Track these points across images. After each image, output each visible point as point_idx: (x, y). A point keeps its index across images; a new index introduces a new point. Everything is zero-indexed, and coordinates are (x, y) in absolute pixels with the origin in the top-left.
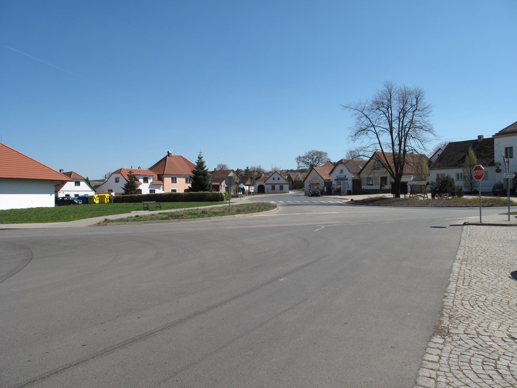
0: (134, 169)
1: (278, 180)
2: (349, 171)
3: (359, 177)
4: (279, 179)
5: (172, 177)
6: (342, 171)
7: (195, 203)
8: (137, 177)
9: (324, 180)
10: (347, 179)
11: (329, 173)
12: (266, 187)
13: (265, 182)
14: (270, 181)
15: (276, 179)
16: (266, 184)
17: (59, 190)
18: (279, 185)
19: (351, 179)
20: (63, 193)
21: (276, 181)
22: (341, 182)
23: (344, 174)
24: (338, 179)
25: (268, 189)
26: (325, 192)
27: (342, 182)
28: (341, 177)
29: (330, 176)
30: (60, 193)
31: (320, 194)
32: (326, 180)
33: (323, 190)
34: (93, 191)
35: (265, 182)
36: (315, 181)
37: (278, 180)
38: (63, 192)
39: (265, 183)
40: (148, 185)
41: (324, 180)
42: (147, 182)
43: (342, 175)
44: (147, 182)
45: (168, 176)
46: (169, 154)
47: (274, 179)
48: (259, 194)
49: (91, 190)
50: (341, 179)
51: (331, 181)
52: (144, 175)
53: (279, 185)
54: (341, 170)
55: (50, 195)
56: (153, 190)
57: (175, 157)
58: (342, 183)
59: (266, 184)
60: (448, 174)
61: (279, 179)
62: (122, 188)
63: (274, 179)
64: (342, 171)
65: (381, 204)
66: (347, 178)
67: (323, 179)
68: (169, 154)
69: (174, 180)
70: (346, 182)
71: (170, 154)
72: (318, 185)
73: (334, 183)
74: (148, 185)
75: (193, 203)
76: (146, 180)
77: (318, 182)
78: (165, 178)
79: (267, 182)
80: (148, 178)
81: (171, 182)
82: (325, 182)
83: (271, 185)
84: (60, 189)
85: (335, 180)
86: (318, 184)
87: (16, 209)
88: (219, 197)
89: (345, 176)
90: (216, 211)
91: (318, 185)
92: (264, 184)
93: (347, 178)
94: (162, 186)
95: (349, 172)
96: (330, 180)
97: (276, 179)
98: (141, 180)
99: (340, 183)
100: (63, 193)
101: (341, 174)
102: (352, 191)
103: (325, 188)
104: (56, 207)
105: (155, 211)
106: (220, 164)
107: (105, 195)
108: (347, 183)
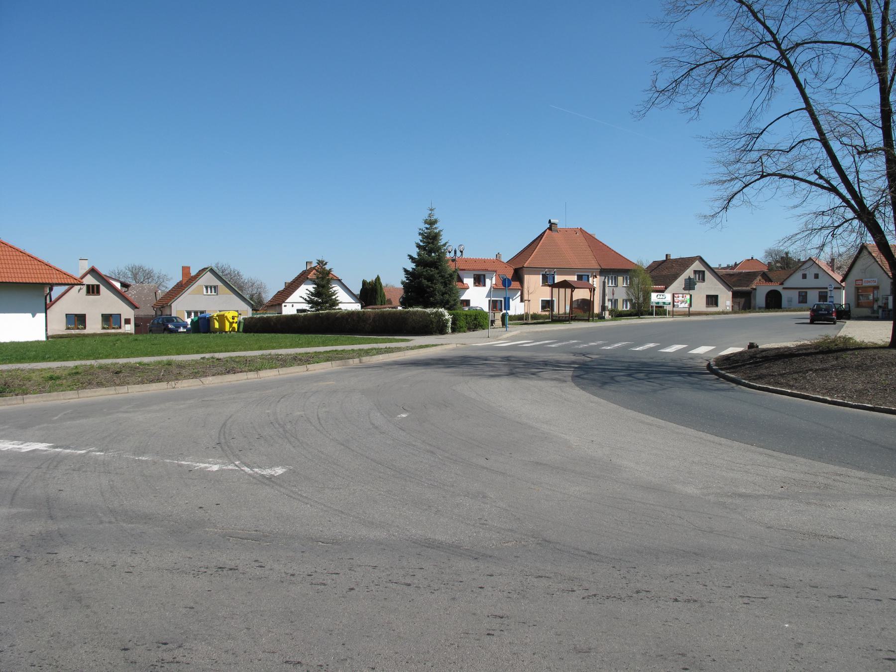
0: (466, 258)
1: (803, 278)
4: (816, 276)
5: (577, 275)
7: (336, 336)
8: (460, 273)
12: (785, 295)
13: (782, 284)
14: (796, 280)
15: (810, 276)
16: (784, 288)
17: (284, 302)
18: (797, 292)
20: (293, 306)
25: (790, 301)
26: (891, 310)
30: (285, 306)
31: (834, 317)
33: (886, 304)
34: (356, 303)
35: (782, 284)
37: (803, 278)
38: (291, 304)
39: (781, 287)
40: (484, 290)
42: (484, 285)
44: (484, 285)
45: (534, 271)
46: (552, 226)
47: (804, 276)
49: (354, 301)
52: (474, 270)
55: (30, 315)
56: (497, 300)
57: (566, 230)
59: (784, 288)
60: (409, 256)
61: (816, 276)
62: (301, 297)
63: (804, 276)
65: (734, 356)
68: (552, 226)
71: (553, 225)
74: (484, 290)
75: (304, 337)
76: (479, 280)
77: (875, 284)
78: (525, 276)
79: (786, 285)
80: (486, 276)
81: (541, 285)
83: (797, 292)
84: (286, 299)
86: (876, 288)
87: (27, 342)
88: (432, 322)
90: (58, 373)
91: (875, 292)
92: (779, 288)
94: (519, 293)
98: (469, 281)
100: (293, 306)
103: (891, 299)
104: (140, 337)
105: (233, 353)
106: (770, 249)
107: (224, 315)
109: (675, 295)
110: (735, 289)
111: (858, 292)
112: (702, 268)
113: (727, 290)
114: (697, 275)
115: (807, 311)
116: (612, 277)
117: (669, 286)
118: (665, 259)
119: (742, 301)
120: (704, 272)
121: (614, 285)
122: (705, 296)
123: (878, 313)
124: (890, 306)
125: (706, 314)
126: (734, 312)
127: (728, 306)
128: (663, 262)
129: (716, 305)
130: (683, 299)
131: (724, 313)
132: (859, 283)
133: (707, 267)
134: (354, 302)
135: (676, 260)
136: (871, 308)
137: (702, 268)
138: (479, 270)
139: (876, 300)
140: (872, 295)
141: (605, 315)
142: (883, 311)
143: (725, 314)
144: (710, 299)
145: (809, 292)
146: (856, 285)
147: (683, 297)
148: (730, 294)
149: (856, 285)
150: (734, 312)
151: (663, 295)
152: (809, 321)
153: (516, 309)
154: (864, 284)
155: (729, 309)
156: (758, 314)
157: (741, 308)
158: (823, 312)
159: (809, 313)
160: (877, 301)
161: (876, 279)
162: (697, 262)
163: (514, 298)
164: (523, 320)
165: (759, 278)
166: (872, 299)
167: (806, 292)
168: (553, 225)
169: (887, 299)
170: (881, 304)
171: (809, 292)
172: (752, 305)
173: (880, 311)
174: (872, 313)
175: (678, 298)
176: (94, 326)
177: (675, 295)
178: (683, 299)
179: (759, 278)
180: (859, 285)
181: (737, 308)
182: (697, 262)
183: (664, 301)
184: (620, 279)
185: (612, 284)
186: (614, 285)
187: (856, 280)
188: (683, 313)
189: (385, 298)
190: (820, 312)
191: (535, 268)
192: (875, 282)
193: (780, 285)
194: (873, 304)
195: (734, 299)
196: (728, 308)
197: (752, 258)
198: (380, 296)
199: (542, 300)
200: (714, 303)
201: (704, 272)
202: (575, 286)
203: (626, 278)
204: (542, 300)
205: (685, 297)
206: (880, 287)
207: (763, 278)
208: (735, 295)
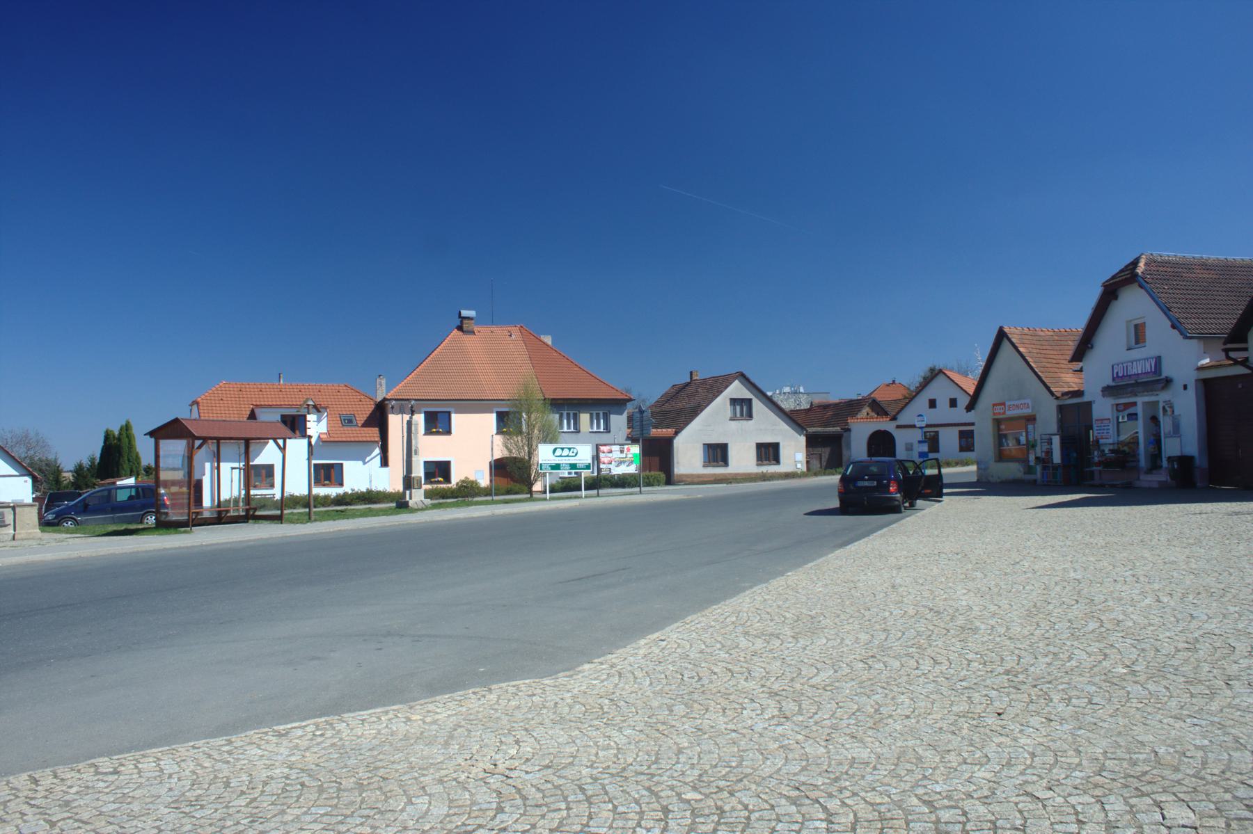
2: (1173, 327)
3: (1236, 362)
5: (426, 413)
6: (1139, 334)
9: (1057, 398)
10: (1168, 382)
11: (1070, 353)
15: (943, 403)
16: (898, 427)
18: (956, 430)
19: (1190, 377)
21: (944, 413)
22: (1134, 404)
23: (1150, 349)
24: (1119, 387)
27: (1141, 400)
28: (1135, 371)
29: (1081, 370)
32: (1064, 394)
33: (1049, 452)
35: (894, 418)
36: (1018, 407)
39: (894, 424)
41: (1057, 398)
43: (1138, 362)
47: (933, 404)
48: (170, 534)
49: (16, 473)
50: (1137, 384)
51: (1086, 399)
52: (279, 406)
53: (956, 430)
54: (1136, 326)
58: (1139, 409)
59: (898, 427)
63: (933, 404)
64: (1139, 334)
66: (1166, 372)
67: (1048, 388)
69: (438, 423)
70: (1162, 397)
72: (1030, 427)
73: (1103, 409)
77: (1026, 411)
82: (1061, 409)
85: (1108, 391)
86: (1031, 419)
89: (1158, 360)
91: (1030, 427)
93: (1166, 372)
95: (1176, 332)
96: (1079, 393)
97: (943, 403)
99: (1131, 410)
101: (1136, 354)
102: (1201, 462)
103: (1056, 441)
108: (1169, 407)
109: (602, 448)
110: (811, 430)
111: (999, 429)
112: (746, 394)
113: (797, 432)
114: (738, 408)
115: (972, 464)
116: (568, 415)
117: (682, 429)
118: (689, 381)
119: (826, 452)
120: (750, 401)
121: (572, 430)
122: (725, 442)
123: (1035, 474)
124: (1057, 458)
125: (764, 477)
126: (810, 471)
127: (800, 462)
128: (687, 384)
129: (777, 460)
130: (624, 455)
131: (787, 476)
132: (999, 409)
133: (755, 391)
134: (17, 474)
135: (704, 382)
136: (1023, 462)
137: (746, 394)
138: (291, 406)
139: (1031, 445)
140: (1024, 434)
141: (411, 498)
142: (1044, 468)
143: (769, 480)
144: (763, 449)
145: (942, 431)
146: (994, 414)
147: (622, 452)
148: (803, 439)
149: (994, 414)
150: (810, 471)
151: (570, 449)
152: (835, 503)
153: (370, 482)
154: (1009, 413)
155: (802, 467)
156: (753, 484)
157: (824, 464)
158: (866, 484)
159: (974, 468)
160: (1034, 446)
161: (1029, 401)
162: (736, 383)
163: (368, 459)
164: (491, 495)
165: (866, 410)
166: (1025, 442)
167: (937, 433)
168: (465, 321)
169: (1050, 442)
170: (1039, 455)
171: (942, 431)
172: (845, 459)
173: (1039, 468)
174: (1025, 473)
175: (610, 455)
176: (742, 460)
177: (602, 448)
178: (624, 455)
179: (866, 410)
180: (999, 414)
181: (816, 464)
182: (736, 383)
183: (572, 460)
184: (584, 418)
185: (569, 427)
186: (572, 430)
187: (994, 405)
188: (712, 479)
189: (139, 463)
190: (860, 484)
191: (426, 400)
192: (1028, 407)
193: (891, 420)
194: (1028, 453)
195: (811, 449)
196: (799, 466)
197: (894, 382)
198: (129, 460)
199: (425, 462)
200: (771, 458)
201: (750, 401)
202: (196, 434)
203: (598, 415)
204: (425, 462)
205: (629, 450)
206: (1038, 417)
207: (873, 410)
208: (813, 442)
